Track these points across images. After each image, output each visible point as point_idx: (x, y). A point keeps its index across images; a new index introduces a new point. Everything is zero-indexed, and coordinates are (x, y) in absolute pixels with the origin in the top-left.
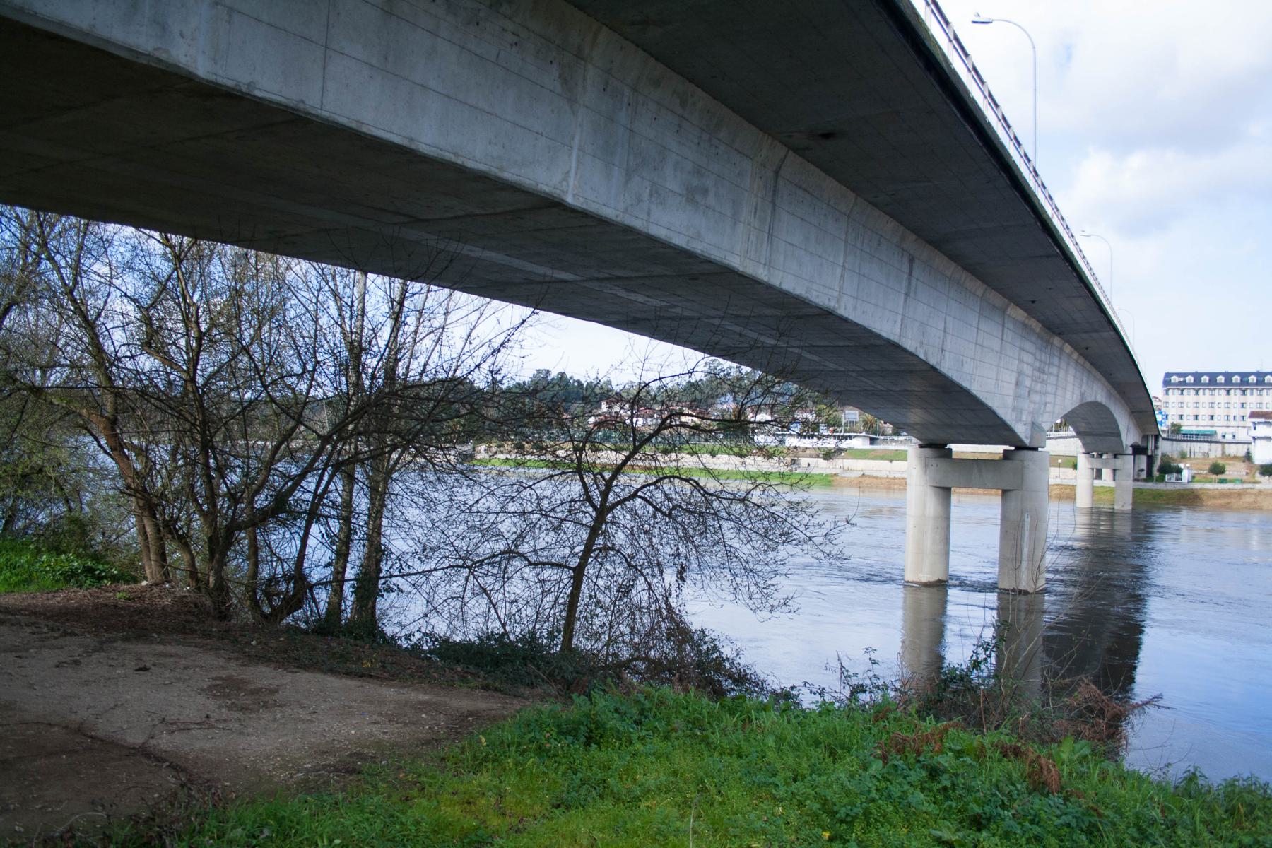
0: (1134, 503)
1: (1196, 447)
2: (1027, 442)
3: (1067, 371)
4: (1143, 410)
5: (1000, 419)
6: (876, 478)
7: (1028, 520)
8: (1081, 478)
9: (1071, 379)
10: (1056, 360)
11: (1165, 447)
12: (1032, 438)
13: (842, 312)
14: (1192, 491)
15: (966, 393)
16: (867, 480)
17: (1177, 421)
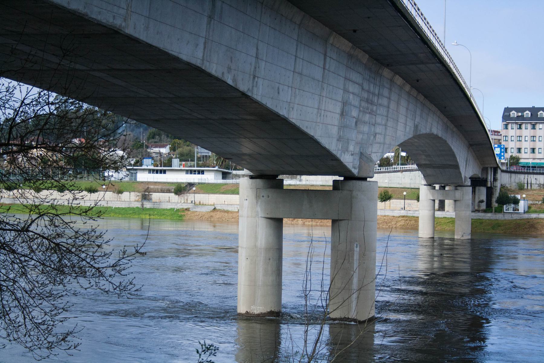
0: (472, 233)
1: (532, 179)
2: (355, 172)
3: (398, 104)
4: (478, 140)
5: (325, 148)
6: (227, 212)
7: (357, 250)
8: (422, 210)
9: (402, 110)
10: (386, 92)
11: (504, 179)
12: (360, 167)
13: (130, 31)
14: (528, 220)
15: (285, 121)
16: (218, 215)
17: (515, 154)
